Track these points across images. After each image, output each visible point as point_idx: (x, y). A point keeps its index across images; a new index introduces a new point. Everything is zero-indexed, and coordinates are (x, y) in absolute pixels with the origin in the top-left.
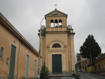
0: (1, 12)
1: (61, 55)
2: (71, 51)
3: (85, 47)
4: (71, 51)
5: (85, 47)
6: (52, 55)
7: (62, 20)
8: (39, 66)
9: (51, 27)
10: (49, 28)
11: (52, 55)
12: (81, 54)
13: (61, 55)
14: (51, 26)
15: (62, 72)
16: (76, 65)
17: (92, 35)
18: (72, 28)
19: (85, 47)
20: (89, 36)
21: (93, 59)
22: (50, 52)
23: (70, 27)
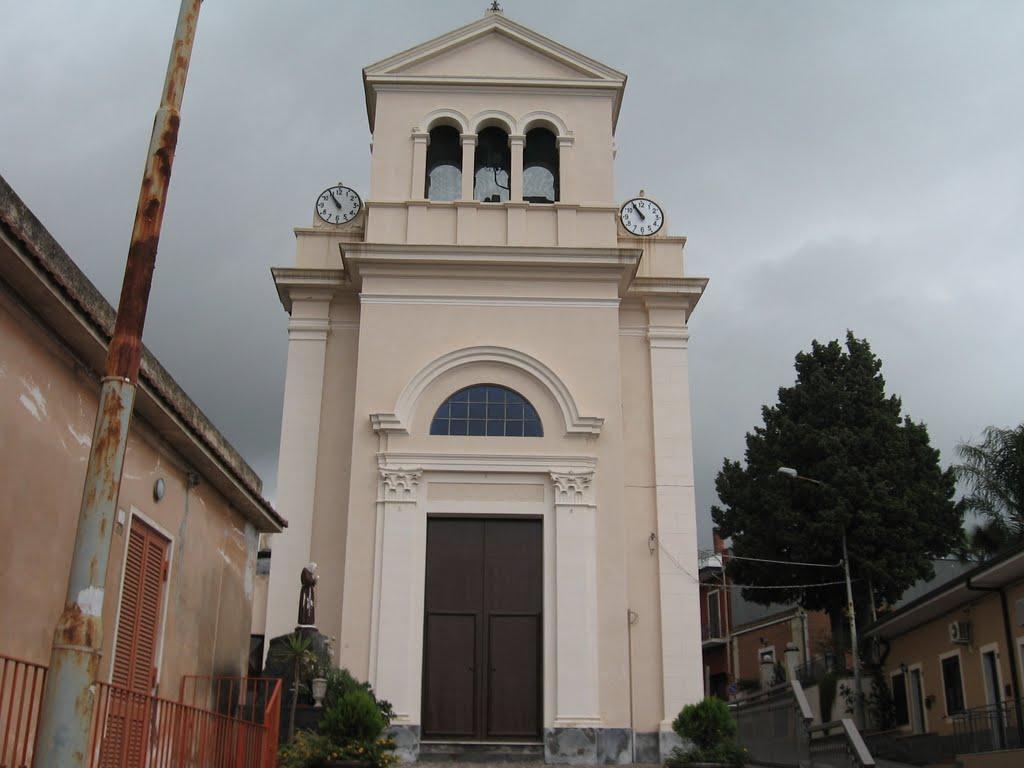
0: (3, 176)
1: (538, 520)
2: (654, 487)
3: (793, 472)
4: (658, 483)
5: (793, 472)
6: (432, 519)
7: (562, 135)
8: (126, 706)
9: (342, 268)
10: (455, 207)
11: (432, 519)
12: (735, 571)
13: (538, 520)
14: (337, 268)
15: (545, 734)
16: (927, 581)
17: (850, 335)
18: (672, 231)
19: (787, 476)
20: (819, 365)
21: (769, 701)
22: (408, 484)
23: (642, 217)
